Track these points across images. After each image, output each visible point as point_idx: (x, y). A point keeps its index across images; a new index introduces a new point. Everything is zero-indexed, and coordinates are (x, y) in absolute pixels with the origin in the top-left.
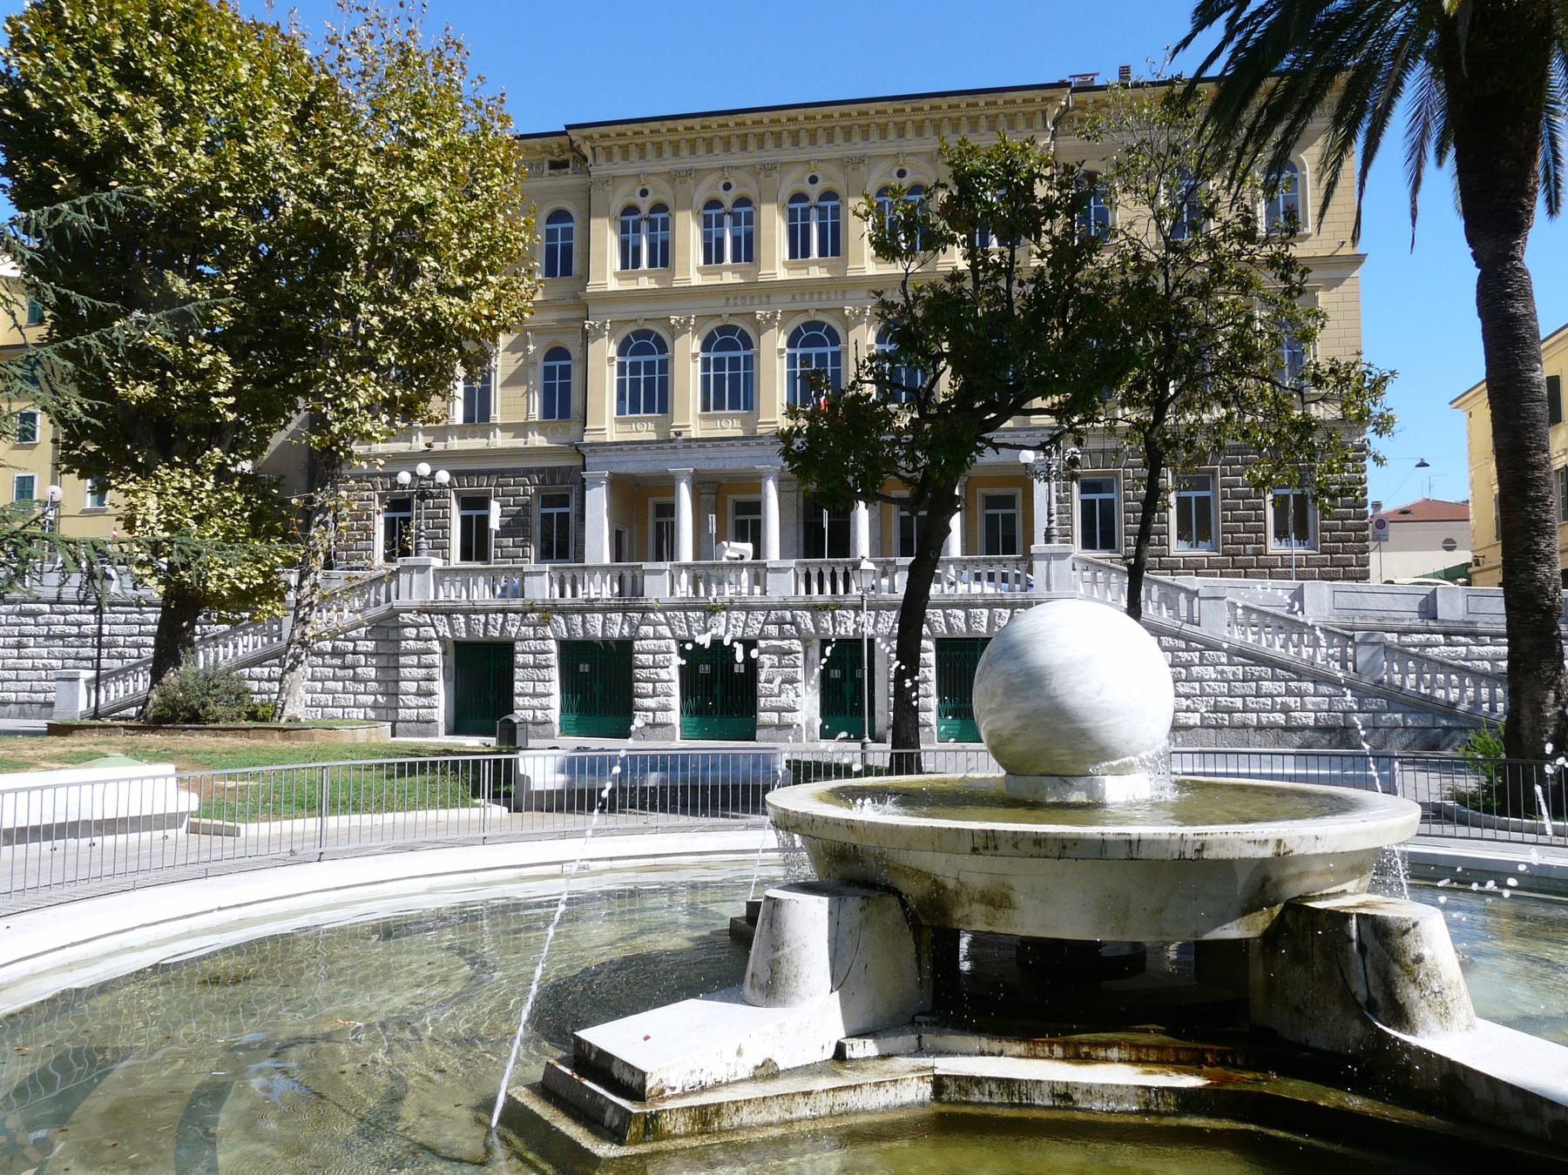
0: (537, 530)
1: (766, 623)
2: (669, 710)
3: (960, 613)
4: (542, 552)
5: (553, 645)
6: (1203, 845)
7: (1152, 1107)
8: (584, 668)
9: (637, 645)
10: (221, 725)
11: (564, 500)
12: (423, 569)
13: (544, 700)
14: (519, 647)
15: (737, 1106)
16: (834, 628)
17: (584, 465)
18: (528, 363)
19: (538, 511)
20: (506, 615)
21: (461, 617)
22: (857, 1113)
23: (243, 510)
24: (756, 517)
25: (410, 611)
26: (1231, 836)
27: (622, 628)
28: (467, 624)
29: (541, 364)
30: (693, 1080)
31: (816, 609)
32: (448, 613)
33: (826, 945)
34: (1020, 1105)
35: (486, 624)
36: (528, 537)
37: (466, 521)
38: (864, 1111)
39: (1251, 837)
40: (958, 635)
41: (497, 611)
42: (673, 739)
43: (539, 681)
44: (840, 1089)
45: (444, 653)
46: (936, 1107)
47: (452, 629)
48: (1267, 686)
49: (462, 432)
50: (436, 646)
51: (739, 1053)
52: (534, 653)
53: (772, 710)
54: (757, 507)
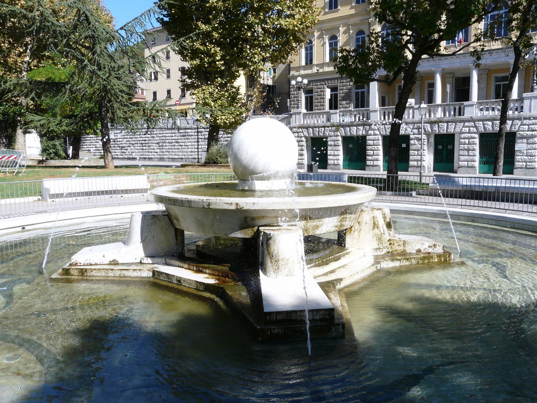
0: (354, 98)
1: (413, 129)
3: (490, 123)
4: (356, 106)
5: (340, 138)
6: (209, 203)
7: (198, 288)
8: (351, 146)
9: (368, 137)
10: (222, 164)
12: (299, 113)
13: (337, 157)
15: (92, 270)
16: (439, 130)
18: (350, 37)
19: (354, 91)
20: (325, 128)
21: (311, 129)
22: (128, 277)
23: (228, 97)
25: (296, 128)
26: (218, 201)
27: (363, 132)
28: (313, 131)
29: (355, 37)
30: (88, 262)
31: (432, 123)
32: (307, 128)
33: (140, 229)
34: (170, 282)
35: (319, 131)
36: (351, 101)
37: (306, 98)
38: (131, 277)
39: (225, 201)
40: (488, 132)
41: (322, 127)
42: (380, 171)
43: (336, 150)
44: (123, 270)
45: (307, 141)
46: (152, 279)
47: (308, 134)
49: (304, 68)
50: (304, 139)
51: (104, 256)
52: (334, 141)
53: (414, 161)
54: (432, 85)
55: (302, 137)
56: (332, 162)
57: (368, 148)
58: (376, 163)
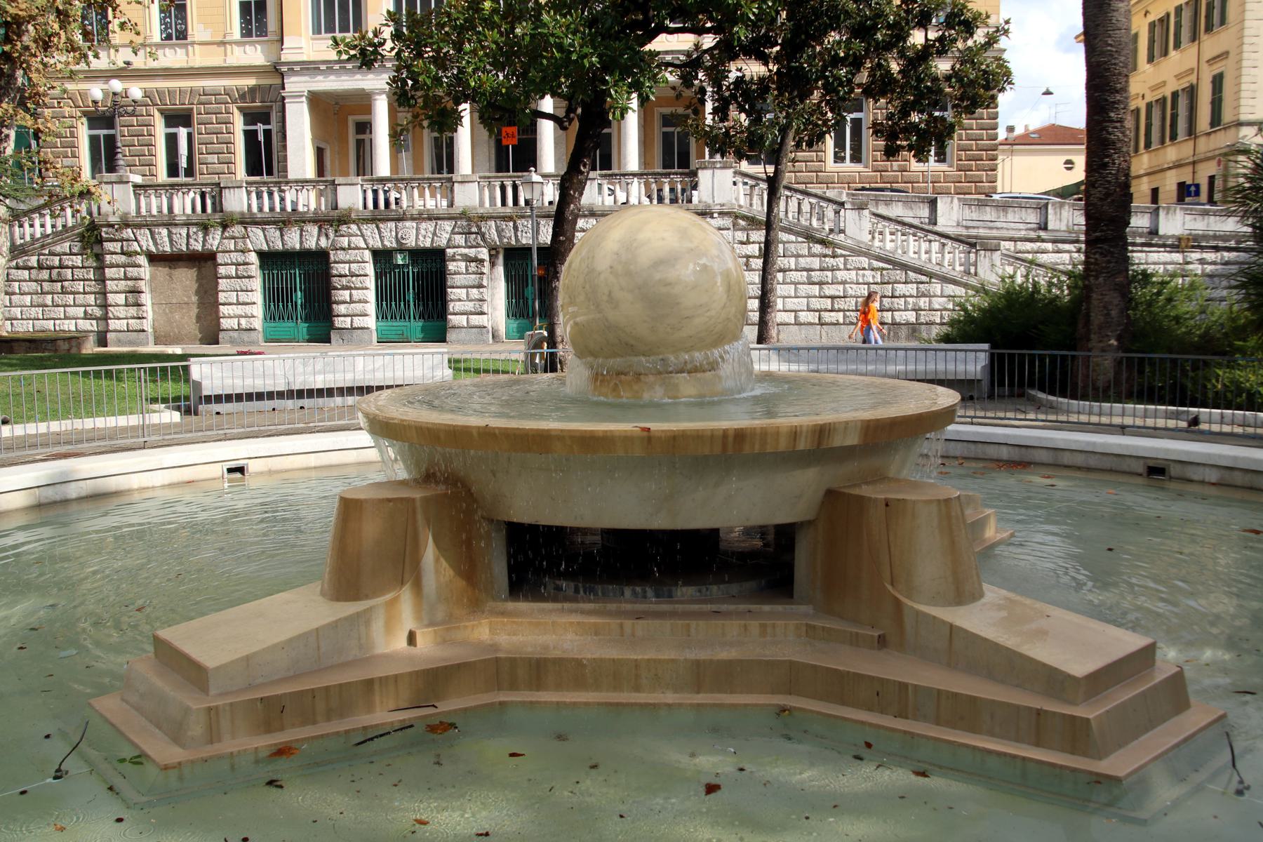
3: (164, 232)
5: (253, 258)
14: (220, 258)
16: (516, 236)
17: (283, 84)
43: (242, 291)
48: (901, 289)
54: (365, 127)
55: (137, 253)
56: (233, 323)
57: (336, 281)
58: (358, 322)
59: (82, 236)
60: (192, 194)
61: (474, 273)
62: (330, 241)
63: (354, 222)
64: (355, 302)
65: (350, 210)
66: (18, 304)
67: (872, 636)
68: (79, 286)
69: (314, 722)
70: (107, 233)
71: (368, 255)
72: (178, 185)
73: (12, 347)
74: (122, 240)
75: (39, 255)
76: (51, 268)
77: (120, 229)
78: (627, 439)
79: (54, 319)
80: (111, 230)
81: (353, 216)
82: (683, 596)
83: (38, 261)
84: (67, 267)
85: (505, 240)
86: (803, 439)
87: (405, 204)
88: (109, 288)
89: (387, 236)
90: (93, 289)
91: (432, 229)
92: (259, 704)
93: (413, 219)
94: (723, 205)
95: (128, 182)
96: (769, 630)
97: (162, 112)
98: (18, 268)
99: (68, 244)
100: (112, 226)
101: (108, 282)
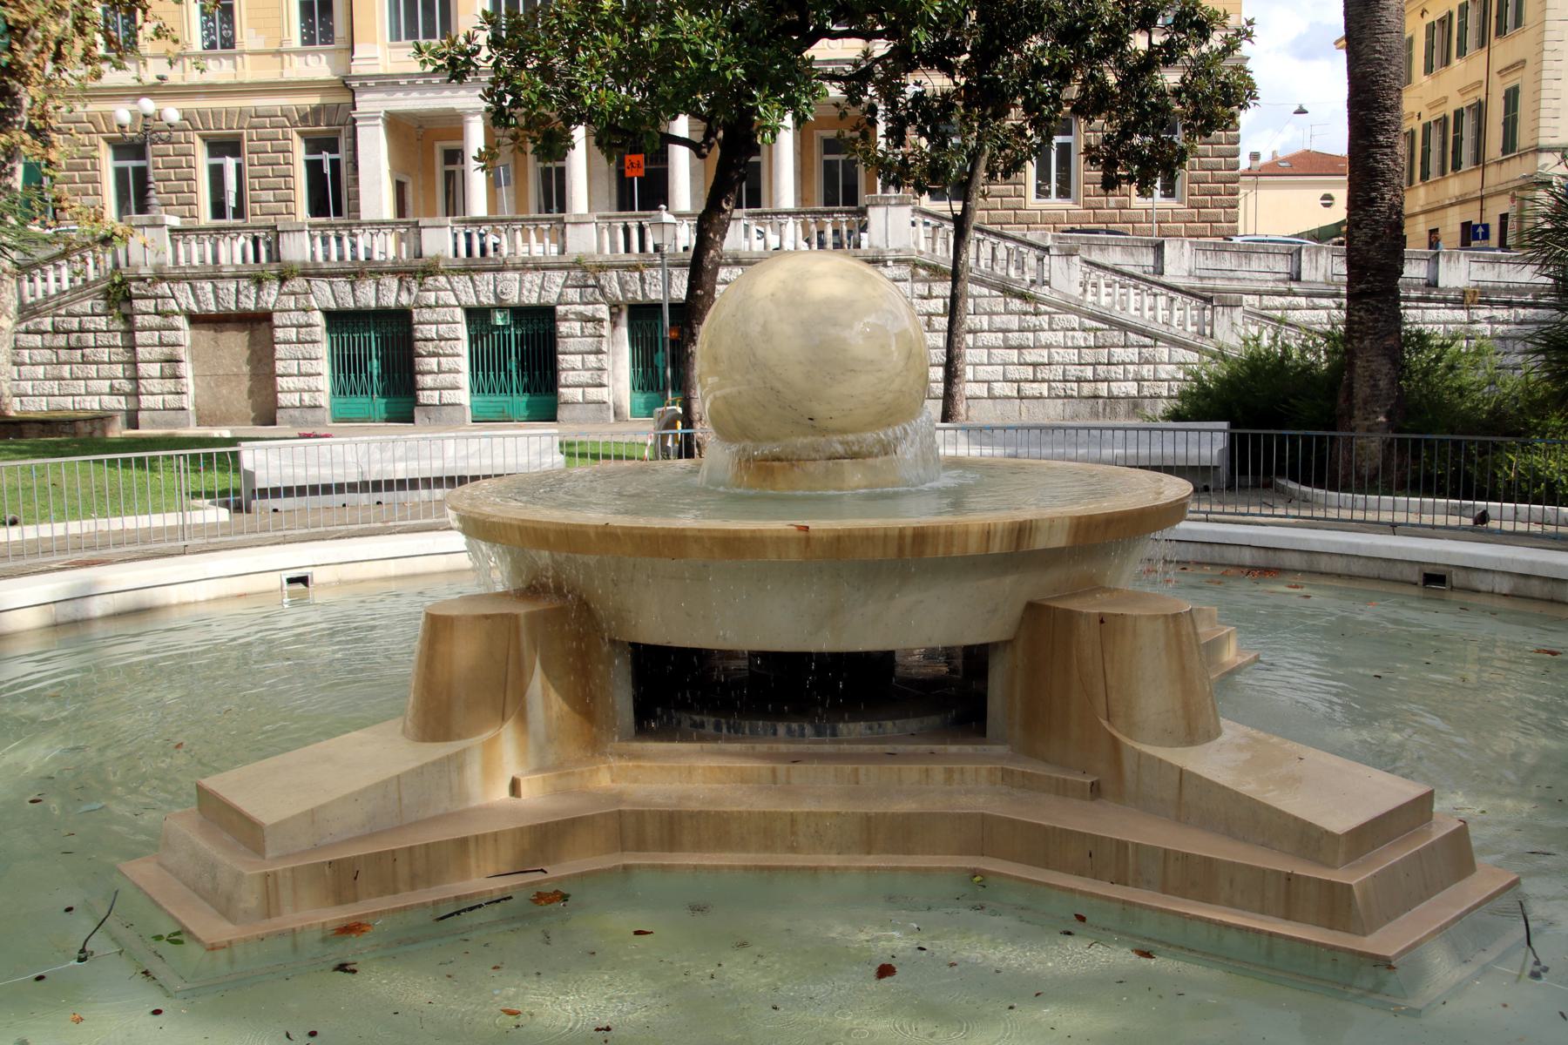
2: (458, 388)
3: (208, 286)
5: (318, 318)
11: (332, 146)
14: (278, 319)
16: (643, 290)
17: (354, 103)
24: (559, 164)
43: (305, 359)
48: (1119, 354)
55: (174, 313)
56: (294, 399)
57: (420, 347)
58: (448, 397)
59: (107, 294)
60: (241, 240)
61: (591, 336)
62: (413, 297)
63: (442, 273)
64: (444, 372)
65: (438, 258)
66: (29, 376)
67: (1084, 784)
68: (104, 354)
69: (395, 891)
70: (137, 289)
71: (460, 314)
72: (225, 229)
73: (21, 430)
74: (156, 297)
75: (54, 316)
76: (68, 332)
77: (154, 283)
78: (780, 541)
79: (73, 395)
80: (142, 284)
81: (441, 266)
82: (849, 734)
83: (53, 323)
84: (89, 331)
85: (630, 295)
86: (998, 540)
87: (505, 250)
88: (140, 356)
89: (483, 291)
90: (120, 358)
91: (539, 282)
92: (326, 868)
93: (515, 269)
94: (899, 251)
95: (163, 225)
96: (956, 776)
97: (204, 138)
98: (28, 332)
99: (89, 303)
100: (144, 280)
101: (139, 350)
